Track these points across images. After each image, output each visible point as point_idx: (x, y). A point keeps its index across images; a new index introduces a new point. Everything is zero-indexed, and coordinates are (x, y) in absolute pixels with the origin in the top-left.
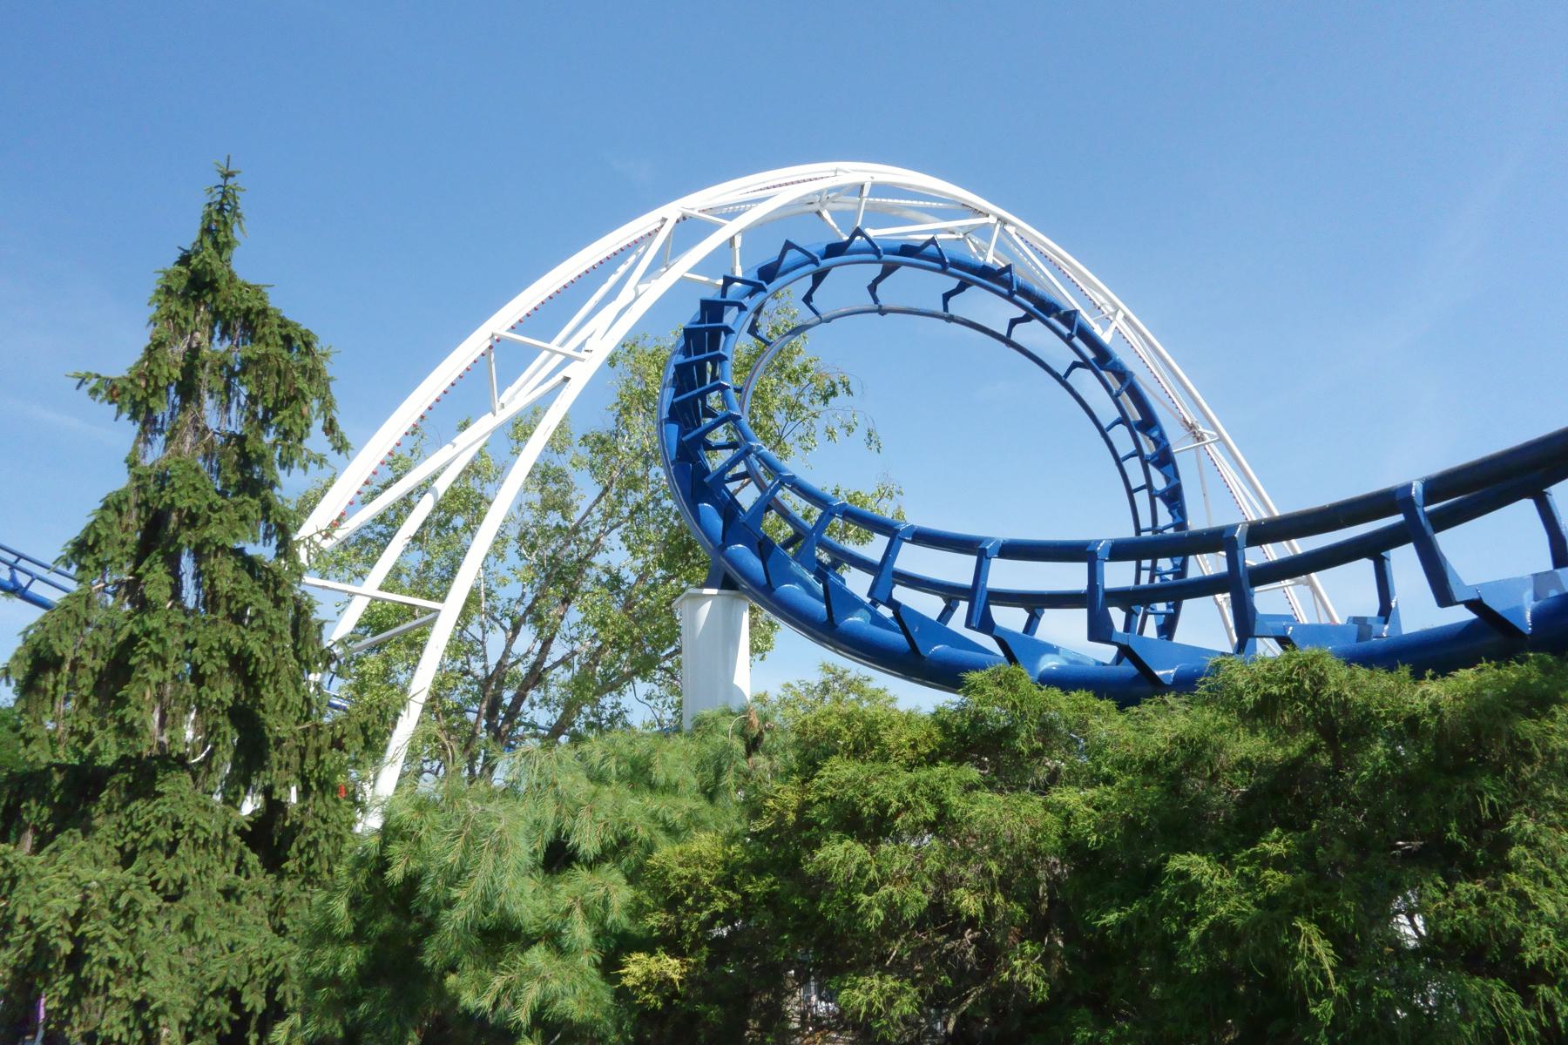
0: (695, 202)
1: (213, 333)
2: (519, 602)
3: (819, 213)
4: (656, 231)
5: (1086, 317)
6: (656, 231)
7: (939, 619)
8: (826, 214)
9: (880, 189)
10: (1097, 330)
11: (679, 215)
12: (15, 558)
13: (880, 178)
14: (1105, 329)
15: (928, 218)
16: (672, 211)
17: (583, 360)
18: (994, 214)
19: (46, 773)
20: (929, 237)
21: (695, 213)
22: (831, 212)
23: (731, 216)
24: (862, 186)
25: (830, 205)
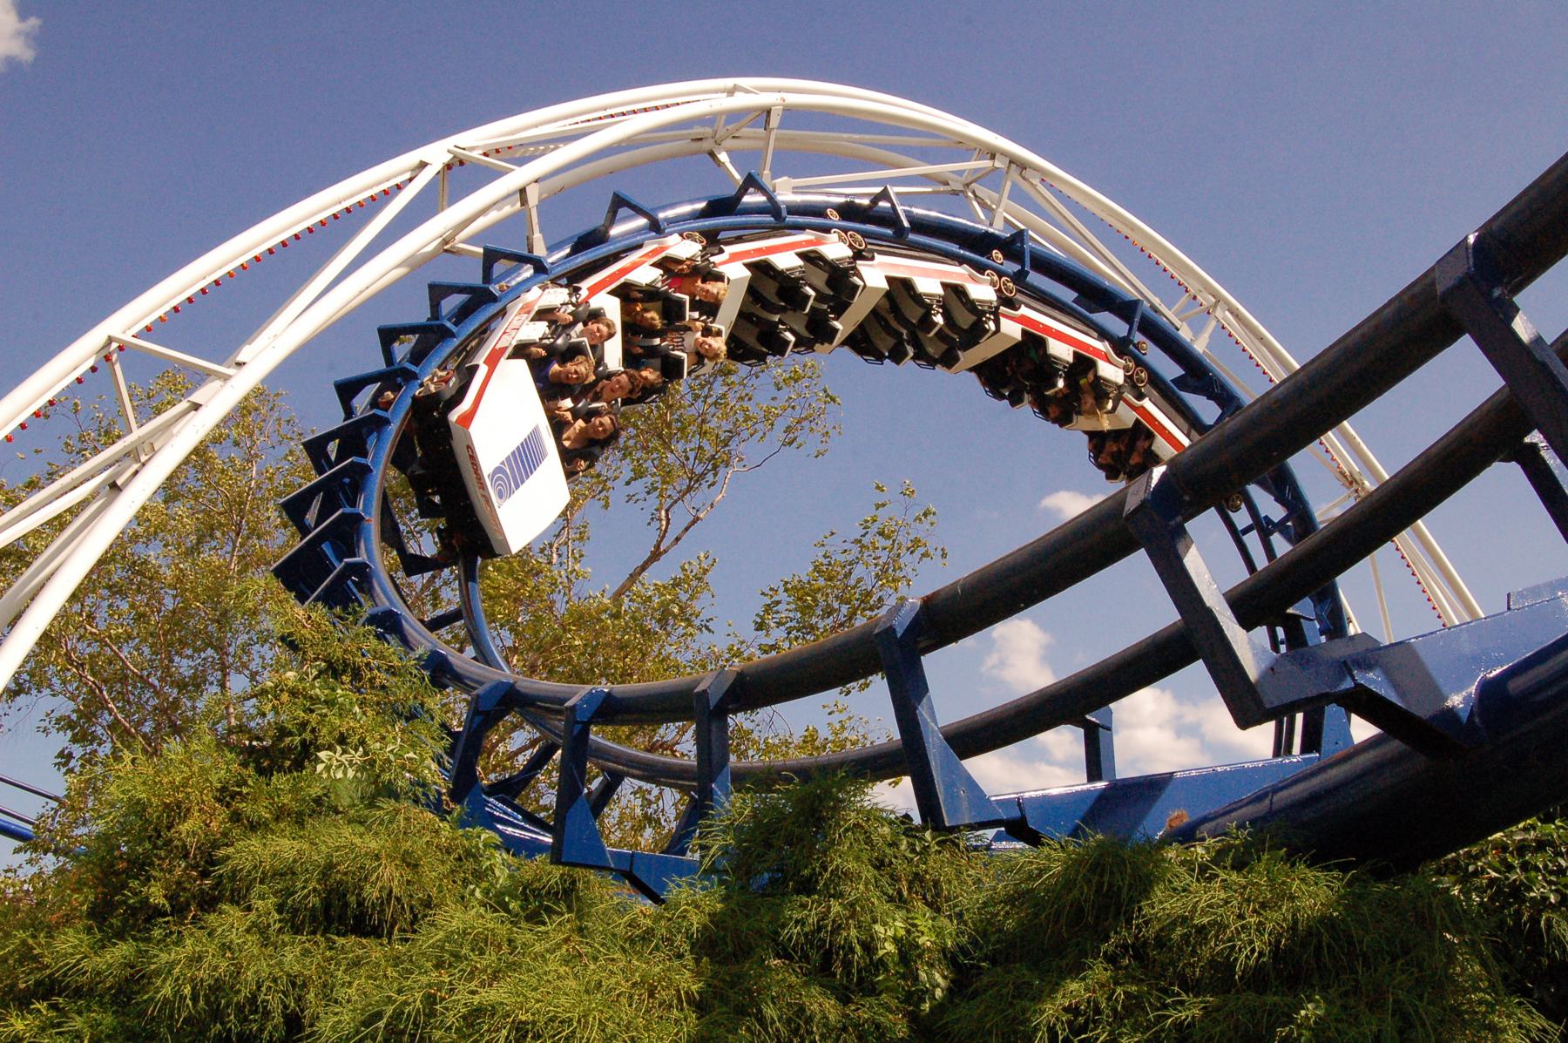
0: (475, 140)
1: (520, 284)
2: (853, 744)
3: (712, 155)
4: (399, 187)
5: (1171, 315)
6: (399, 187)
7: (1277, 753)
8: (723, 157)
9: (796, 116)
10: (1185, 334)
11: (448, 158)
12: (1064, 741)
13: (793, 99)
14: (1197, 332)
15: (903, 159)
16: (437, 154)
17: (226, 378)
18: (1004, 154)
19: (44, 979)
20: (878, 190)
21: (476, 154)
22: (730, 152)
23: (521, 162)
24: (769, 112)
25: (729, 143)
